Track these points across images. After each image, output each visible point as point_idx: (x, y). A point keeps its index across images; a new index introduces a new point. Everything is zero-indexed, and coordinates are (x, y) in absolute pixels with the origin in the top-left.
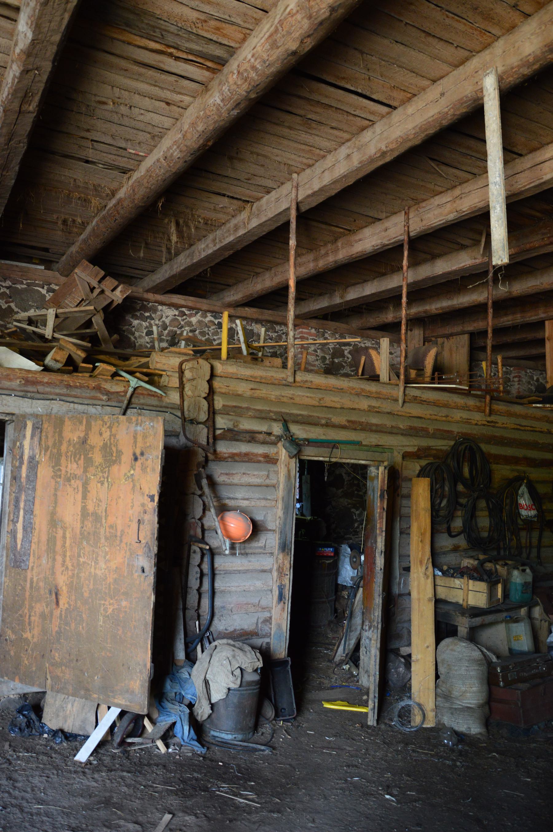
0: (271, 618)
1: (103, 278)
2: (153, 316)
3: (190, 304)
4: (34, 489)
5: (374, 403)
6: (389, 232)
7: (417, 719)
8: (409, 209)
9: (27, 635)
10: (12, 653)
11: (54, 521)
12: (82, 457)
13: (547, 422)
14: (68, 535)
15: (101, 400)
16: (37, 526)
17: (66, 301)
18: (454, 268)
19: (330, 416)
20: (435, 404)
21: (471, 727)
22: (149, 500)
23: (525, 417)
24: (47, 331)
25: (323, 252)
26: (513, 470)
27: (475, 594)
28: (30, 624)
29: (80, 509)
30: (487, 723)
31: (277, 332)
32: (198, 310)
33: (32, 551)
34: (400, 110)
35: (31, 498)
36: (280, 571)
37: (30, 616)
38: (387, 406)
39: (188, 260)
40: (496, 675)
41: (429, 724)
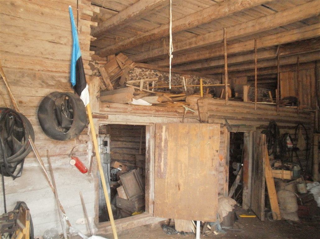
0: (223, 188)
1: (127, 60)
2: (133, 72)
3: (146, 67)
4: (167, 150)
5: (248, 110)
6: (246, 47)
7: (275, 218)
8: (257, 39)
9: (167, 201)
10: (160, 208)
11: (176, 161)
12: (188, 138)
13: (293, 113)
14: (183, 165)
15: (177, 115)
16: (169, 163)
17: (109, 69)
18: (261, 57)
19: (237, 116)
20: (264, 109)
21: (296, 219)
22: (216, 152)
23: (287, 112)
24: (140, 88)
25: (213, 50)
26: (284, 131)
27: (287, 175)
28: (168, 197)
29: (187, 156)
30: (299, 217)
31: (176, 77)
32: (148, 69)
33: (167, 172)
34: (280, 13)
35: (166, 154)
36: (226, 171)
37: (167, 195)
38: (252, 111)
39: (160, 53)
40: (300, 202)
41: (279, 219)
